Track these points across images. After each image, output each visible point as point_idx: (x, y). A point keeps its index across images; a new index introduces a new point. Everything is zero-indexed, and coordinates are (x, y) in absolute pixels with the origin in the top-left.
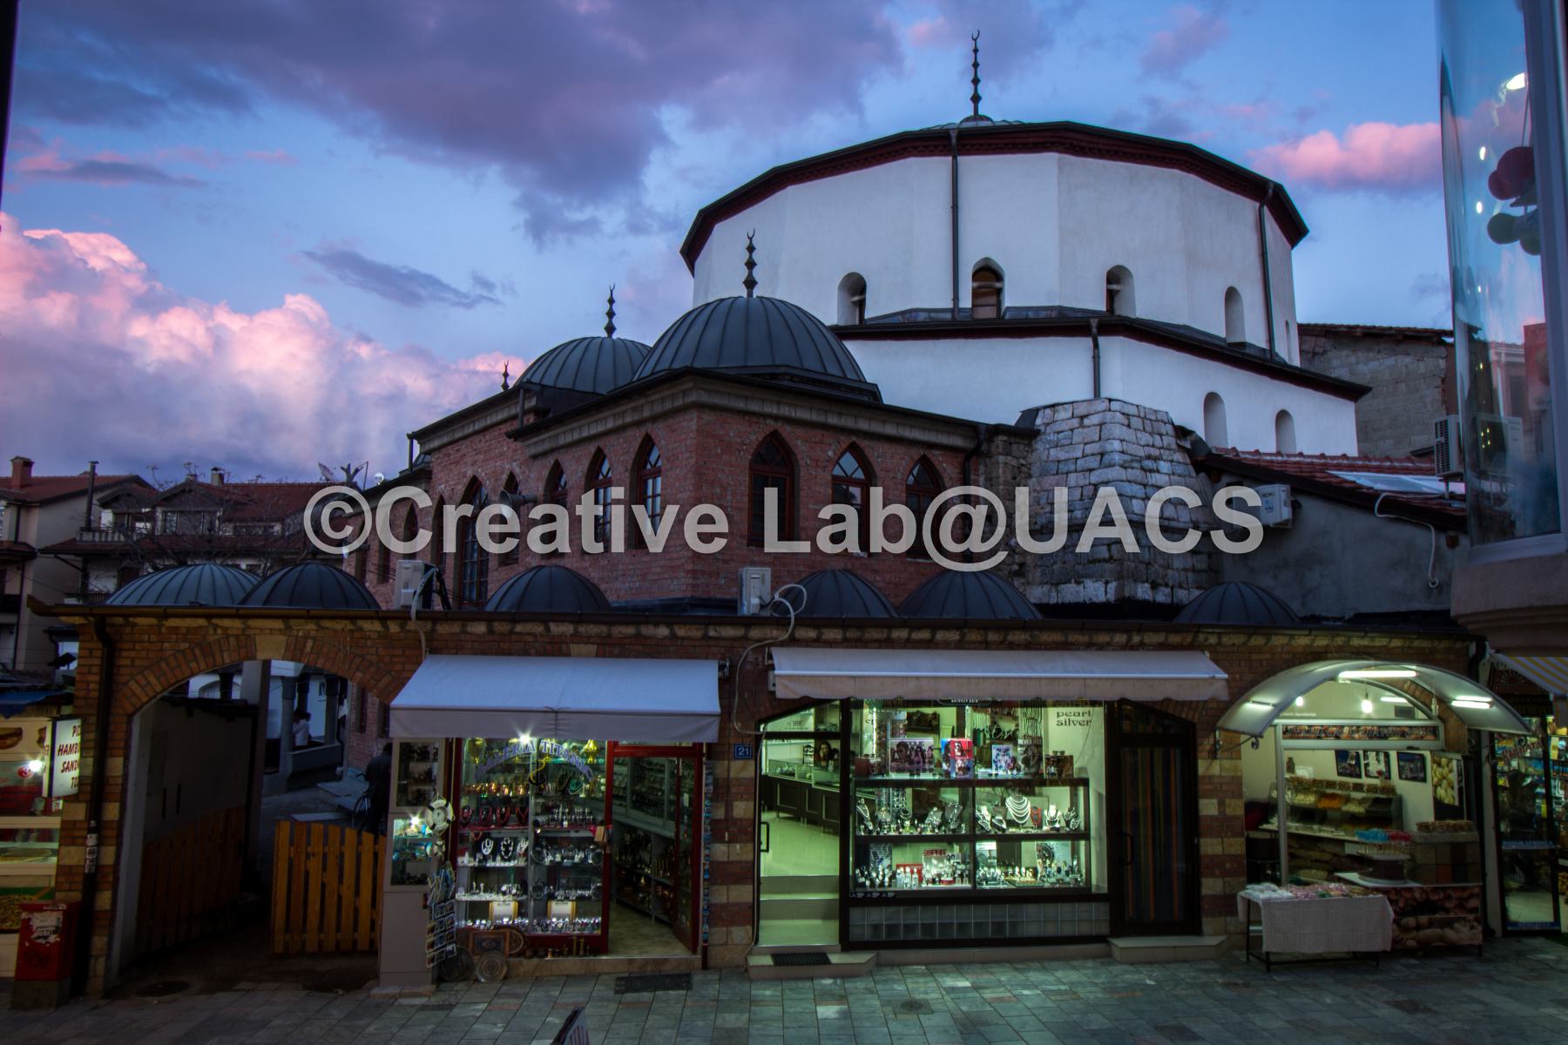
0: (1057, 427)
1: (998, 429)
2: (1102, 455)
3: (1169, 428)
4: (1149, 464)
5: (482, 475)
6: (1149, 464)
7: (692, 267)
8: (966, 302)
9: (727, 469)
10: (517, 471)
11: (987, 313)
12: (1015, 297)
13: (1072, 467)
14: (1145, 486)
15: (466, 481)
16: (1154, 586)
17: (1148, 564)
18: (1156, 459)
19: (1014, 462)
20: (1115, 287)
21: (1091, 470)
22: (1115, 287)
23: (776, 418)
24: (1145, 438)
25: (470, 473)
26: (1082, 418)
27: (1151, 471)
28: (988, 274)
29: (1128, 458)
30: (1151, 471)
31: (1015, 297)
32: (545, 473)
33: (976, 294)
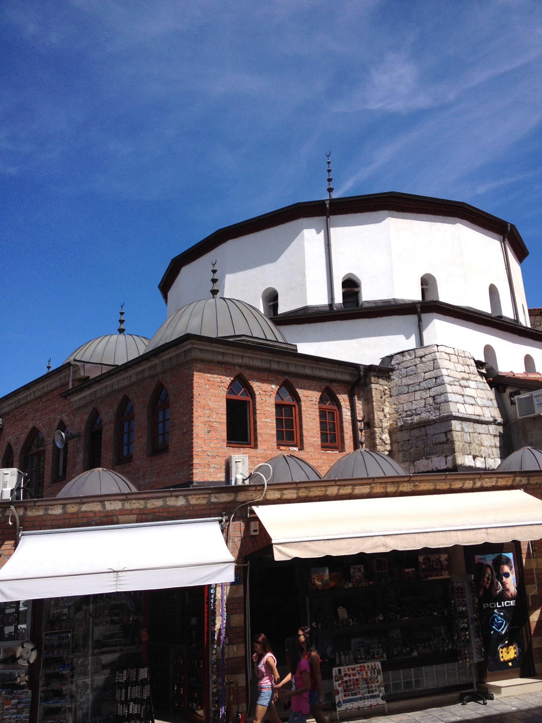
0: (405, 365)
1: (371, 368)
2: (436, 378)
3: (472, 362)
4: (463, 383)
5: (39, 425)
6: (463, 383)
7: (165, 297)
8: (339, 299)
9: (213, 398)
10: (66, 419)
11: (351, 308)
12: (369, 294)
13: (417, 388)
14: (463, 395)
15: (27, 431)
16: (474, 457)
17: (470, 443)
18: (468, 380)
19: (381, 388)
20: (425, 287)
21: (430, 388)
22: (425, 287)
23: (240, 366)
24: (460, 368)
25: (30, 426)
26: (421, 357)
27: (466, 387)
28: (351, 285)
29: (452, 379)
30: (466, 387)
31: (369, 294)
32: (86, 417)
33: (345, 295)
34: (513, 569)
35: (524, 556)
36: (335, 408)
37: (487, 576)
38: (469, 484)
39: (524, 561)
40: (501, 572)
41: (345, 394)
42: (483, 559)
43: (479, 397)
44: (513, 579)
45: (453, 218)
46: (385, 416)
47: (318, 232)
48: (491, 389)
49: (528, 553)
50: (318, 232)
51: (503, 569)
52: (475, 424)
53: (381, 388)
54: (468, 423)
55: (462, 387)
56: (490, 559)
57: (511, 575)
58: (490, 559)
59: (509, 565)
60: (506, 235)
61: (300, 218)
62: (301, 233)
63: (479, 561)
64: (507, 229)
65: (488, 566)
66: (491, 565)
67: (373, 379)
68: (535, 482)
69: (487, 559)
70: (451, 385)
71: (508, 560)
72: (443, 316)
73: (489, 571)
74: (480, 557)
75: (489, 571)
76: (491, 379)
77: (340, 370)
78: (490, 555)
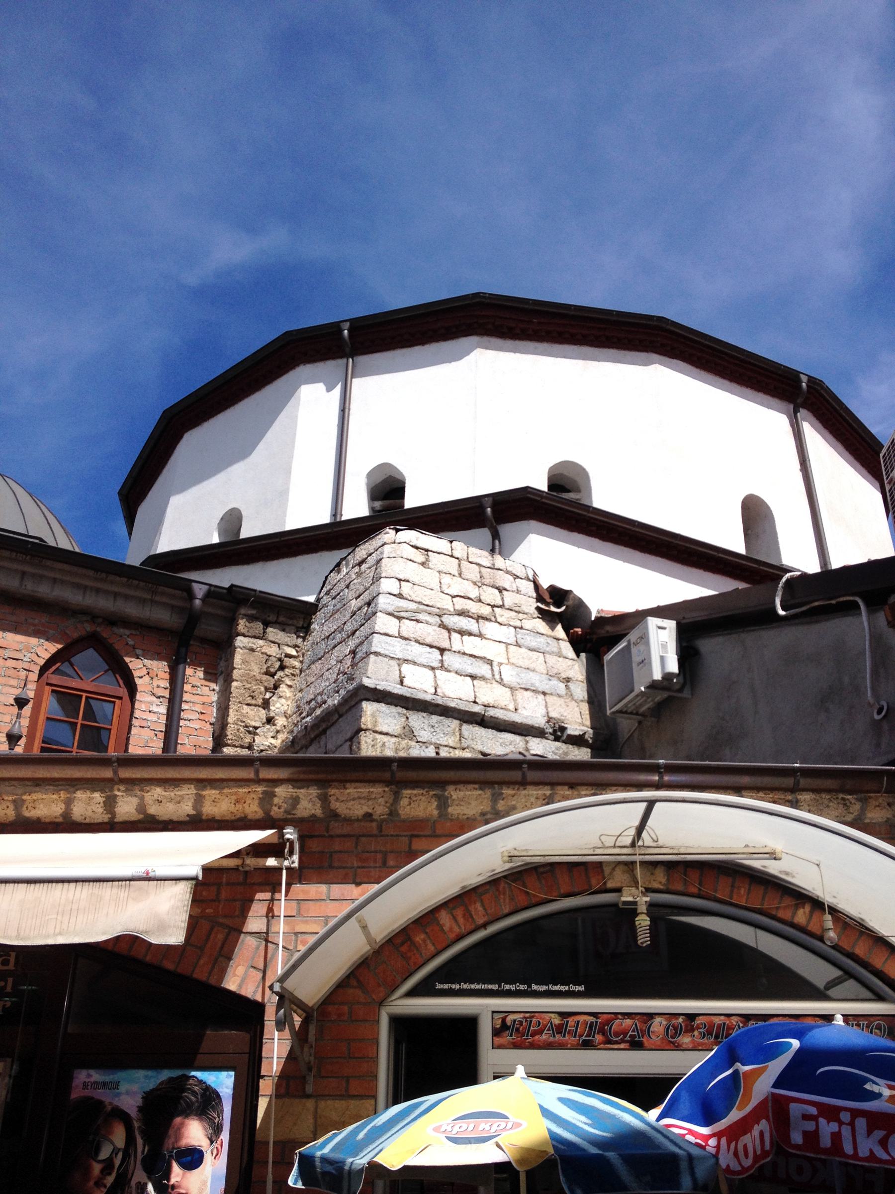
12: (415, 498)
34: (225, 1136)
35: (266, 1087)
36: (123, 692)
37: (104, 1154)
38: (88, 804)
39: (263, 1104)
40: (169, 1143)
41: (160, 659)
42: (104, 1085)
43: (509, 662)
44: (214, 1178)
45: (643, 355)
46: (270, 721)
47: (329, 389)
48: (578, 656)
49: (285, 1077)
50: (329, 389)
51: (179, 1136)
52: (465, 727)
53: (273, 650)
54: (435, 718)
55: (449, 630)
56: (135, 1087)
57: (208, 1158)
58: (135, 1087)
59: (211, 1121)
60: (800, 401)
61: (298, 365)
62: (297, 394)
63: (88, 1093)
64: (801, 386)
65: (123, 1116)
66: (133, 1113)
67: (242, 625)
68: (358, 810)
69: (123, 1088)
70: (400, 618)
71: (210, 1097)
72: (564, 533)
73: (119, 1137)
74: (96, 1076)
75: (119, 1137)
76: (579, 630)
77: (138, 593)
78: (141, 1074)
